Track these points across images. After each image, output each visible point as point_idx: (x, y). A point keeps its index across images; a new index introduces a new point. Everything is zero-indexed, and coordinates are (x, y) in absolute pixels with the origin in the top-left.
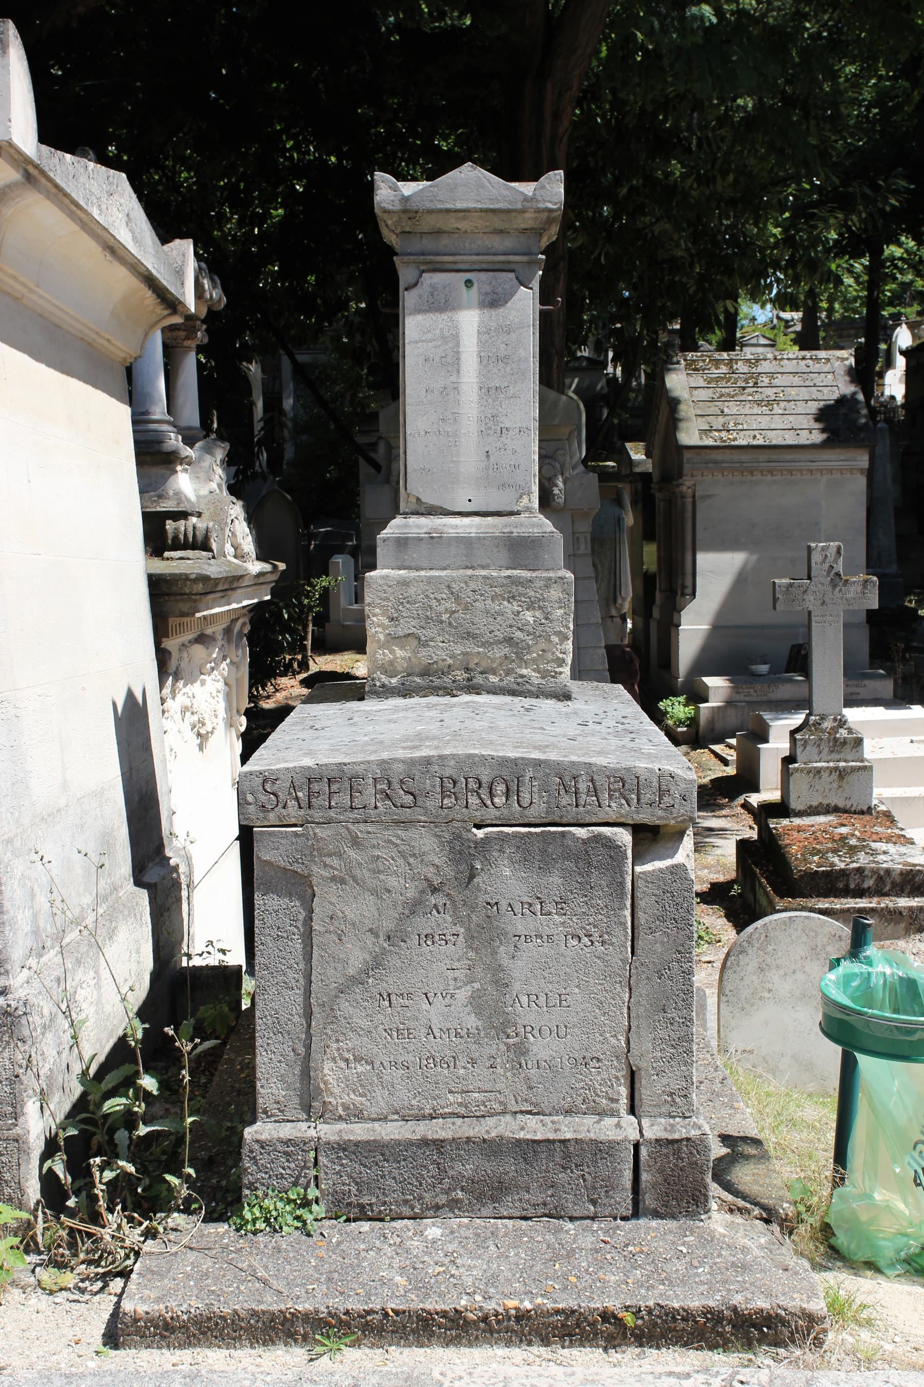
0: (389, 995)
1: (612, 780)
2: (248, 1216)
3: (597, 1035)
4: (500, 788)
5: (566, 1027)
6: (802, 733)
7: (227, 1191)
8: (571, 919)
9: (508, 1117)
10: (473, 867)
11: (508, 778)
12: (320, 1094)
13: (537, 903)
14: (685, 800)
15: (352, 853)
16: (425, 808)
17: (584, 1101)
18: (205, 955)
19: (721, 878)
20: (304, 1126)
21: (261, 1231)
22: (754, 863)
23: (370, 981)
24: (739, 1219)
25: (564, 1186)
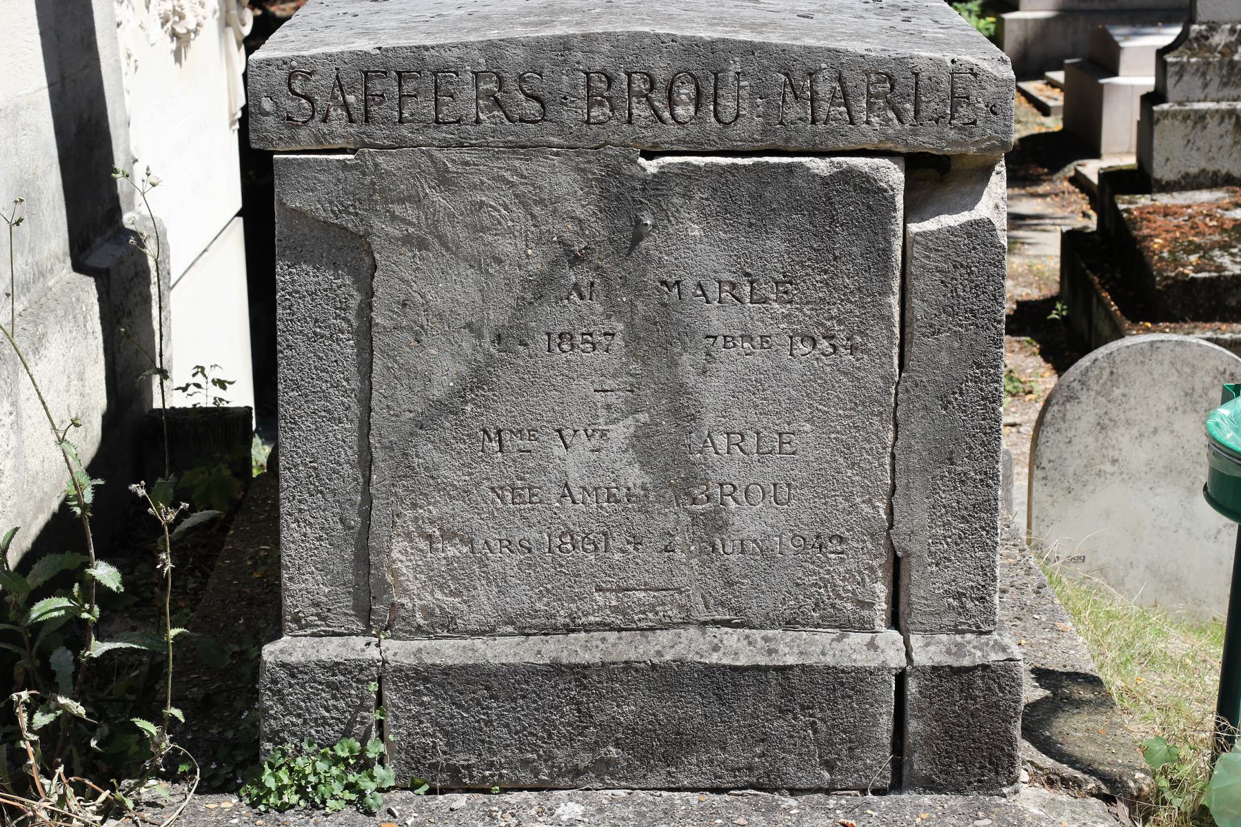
0: (499, 432)
1: (873, 78)
2: (271, 783)
3: (840, 499)
4: (685, 92)
5: (789, 485)
6: (1176, 53)
7: (236, 747)
8: (801, 310)
9: (693, 631)
10: (638, 221)
11: (699, 74)
12: (386, 592)
13: (746, 282)
14: (995, 113)
15: (438, 198)
16: (560, 124)
17: (817, 605)
18: (192, 389)
19: (1034, 294)
20: (359, 642)
21: (292, 807)
22: (1090, 267)
23: (468, 408)
24: (1063, 796)
25: (782, 739)
